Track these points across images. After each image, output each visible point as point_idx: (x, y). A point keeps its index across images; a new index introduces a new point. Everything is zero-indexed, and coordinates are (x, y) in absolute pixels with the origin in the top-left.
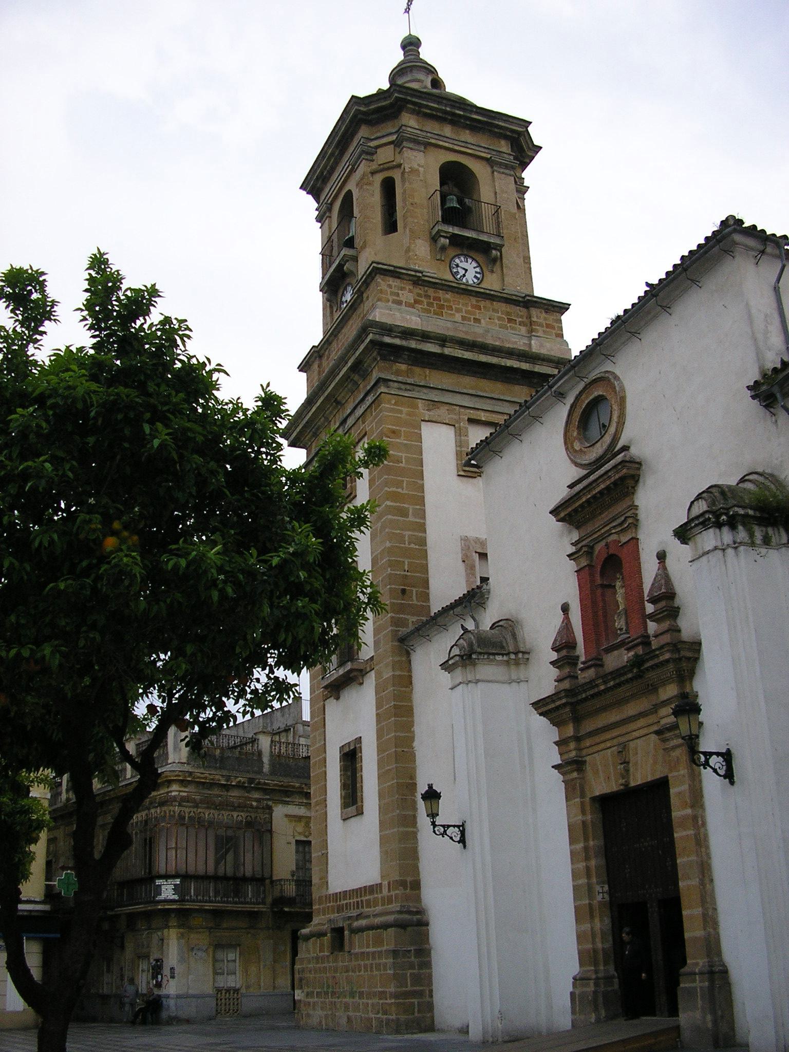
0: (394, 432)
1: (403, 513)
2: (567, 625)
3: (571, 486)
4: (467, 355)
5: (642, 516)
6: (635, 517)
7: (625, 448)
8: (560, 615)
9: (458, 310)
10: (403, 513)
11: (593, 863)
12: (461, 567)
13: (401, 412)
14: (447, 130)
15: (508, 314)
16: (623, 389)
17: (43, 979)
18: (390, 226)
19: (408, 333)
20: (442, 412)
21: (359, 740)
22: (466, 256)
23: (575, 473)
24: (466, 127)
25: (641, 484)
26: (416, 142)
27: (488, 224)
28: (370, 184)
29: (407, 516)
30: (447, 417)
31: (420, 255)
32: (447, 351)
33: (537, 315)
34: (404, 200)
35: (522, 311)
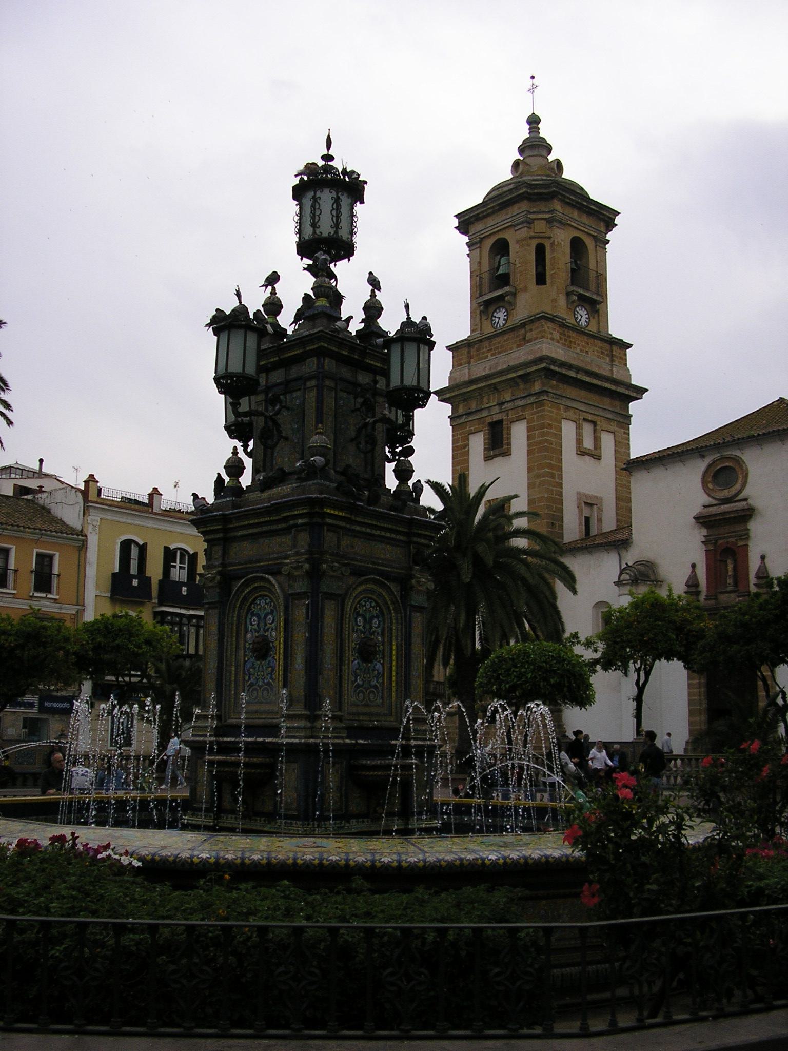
0: (550, 425)
1: (553, 476)
3: (705, 506)
5: (752, 534)
6: (748, 534)
8: (690, 569)
9: (579, 345)
10: (553, 476)
12: (577, 510)
13: (552, 412)
14: (576, 214)
15: (601, 348)
16: (747, 469)
18: (541, 279)
19: (563, 364)
21: (487, 458)
22: (582, 307)
23: (707, 500)
24: (585, 212)
26: (561, 222)
27: (593, 286)
29: (554, 478)
30: (573, 417)
32: (579, 376)
33: (616, 351)
34: (552, 264)
35: (607, 346)
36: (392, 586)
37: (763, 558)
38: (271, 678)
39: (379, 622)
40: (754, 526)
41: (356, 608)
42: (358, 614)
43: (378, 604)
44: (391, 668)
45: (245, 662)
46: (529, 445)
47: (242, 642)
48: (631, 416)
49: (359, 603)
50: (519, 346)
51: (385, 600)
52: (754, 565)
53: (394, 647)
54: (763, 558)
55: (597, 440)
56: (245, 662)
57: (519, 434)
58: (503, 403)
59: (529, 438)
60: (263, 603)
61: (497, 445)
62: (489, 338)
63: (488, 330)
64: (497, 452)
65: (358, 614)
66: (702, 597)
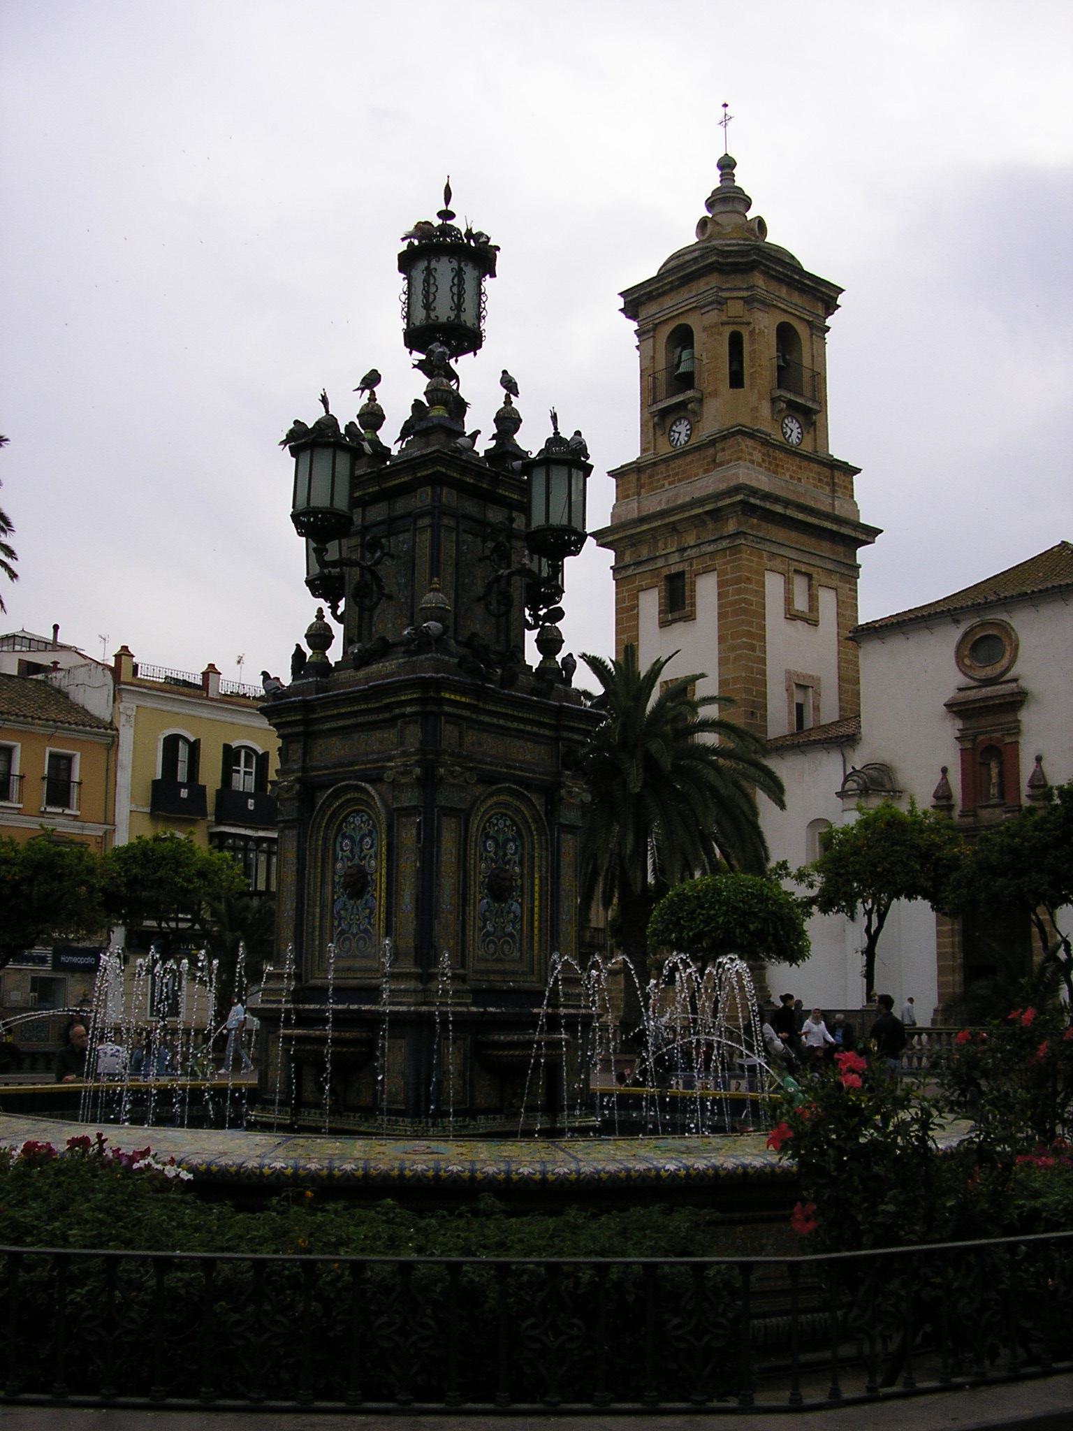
0: (748, 578)
1: (753, 649)
2: (944, 784)
3: (960, 690)
4: (800, 516)
5: (1024, 727)
6: (1018, 728)
7: (1015, 680)
8: (940, 776)
9: (788, 470)
10: (753, 649)
11: (957, 939)
12: (785, 695)
13: (752, 561)
14: (784, 292)
15: (819, 474)
18: (736, 380)
19: (766, 496)
21: (664, 624)
22: (793, 417)
23: (962, 680)
25: (1025, 707)
26: (763, 303)
27: (807, 390)
28: (720, 334)
30: (781, 567)
31: (764, 419)
32: (789, 512)
33: (839, 477)
34: (751, 359)
35: (826, 471)
36: (534, 798)
37: (1039, 759)
38: (369, 923)
39: (517, 847)
40: (1027, 716)
41: (484, 828)
42: (488, 837)
43: (514, 823)
44: (533, 909)
45: (334, 901)
46: (720, 606)
47: (329, 874)
48: (860, 566)
50: (706, 471)
51: (524, 817)
52: (1027, 769)
53: (537, 881)
54: (1039, 759)
55: (813, 599)
56: (334, 901)
57: (706, 591)
58: (685, 549)
60: (358, 821)
61: (677, 606)
62: (665, 461)
63: (665, 449)
64: (677, 615)
65: (488, 837)
66: (956, 813)
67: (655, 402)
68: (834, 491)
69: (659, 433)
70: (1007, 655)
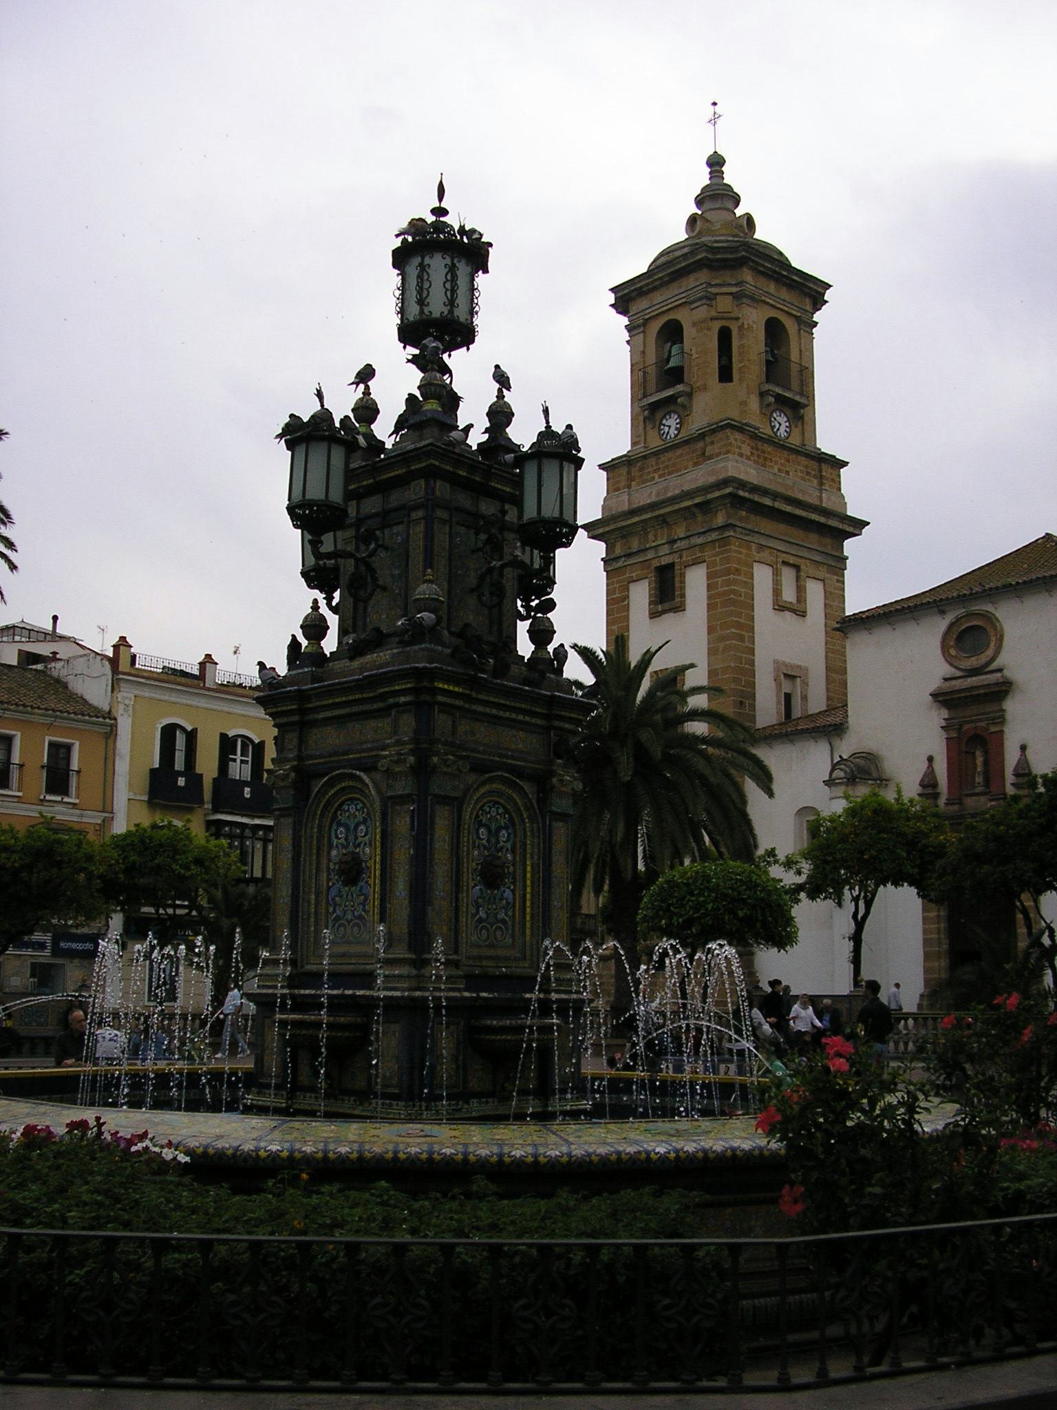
0: (737, 570)
1: (742, 639)
3: (946, 680)
4: (788, 509)
5: (1008, 716)
7: (1000, 670)
8: (926, 764)
9: (776, 463)
10: (742, 639)
11: (942, 925)
12: (773, 684)
13: (741, 553)
14: (772, 288)
15: (807, 467)
17: (934, 993)
18: (725, 374)
19: (755, 489)
20: (765, 555)
21: (654, 615)
22: (781, 411)
23: (948, 670)
24: (785, 284)
26: (752, 298)
27: (795, 384)
29: (743, 641)
30: (770, 559)
31: (753, 413)
32: (777, 505)
33: (827, 470)
34: (740, 354)
35: (814, 464)
36: (527, 786)
37: (1023, 748)
38: (364, 910)
39: (509, 835)
40: (1011, 706)
41: (477, 816)
42: (480, 824)
43: (506, 811)
44: (525, 895)
45: (329, 888)
46: (709, 597)
47: (324, 861)
48: (847, 558)
49: (481, 808)
50: (696, 464)
51: (516, 804)
52: (1011, 758)
53: (529, 868)
54: (1023, 748)
55: (801, 590)
56: (329, 888)
57: (696, 582)
59: (709, 587)
60: (352, 809)
61: (667, 597)
62: (655, 454)
63: (655, 442)
64: (667, 606)
65: (480, 824)
66: (942, 801)
67: (645, 396)
68: (821, 484)
69: (649, 426)
70: (992, 645)
